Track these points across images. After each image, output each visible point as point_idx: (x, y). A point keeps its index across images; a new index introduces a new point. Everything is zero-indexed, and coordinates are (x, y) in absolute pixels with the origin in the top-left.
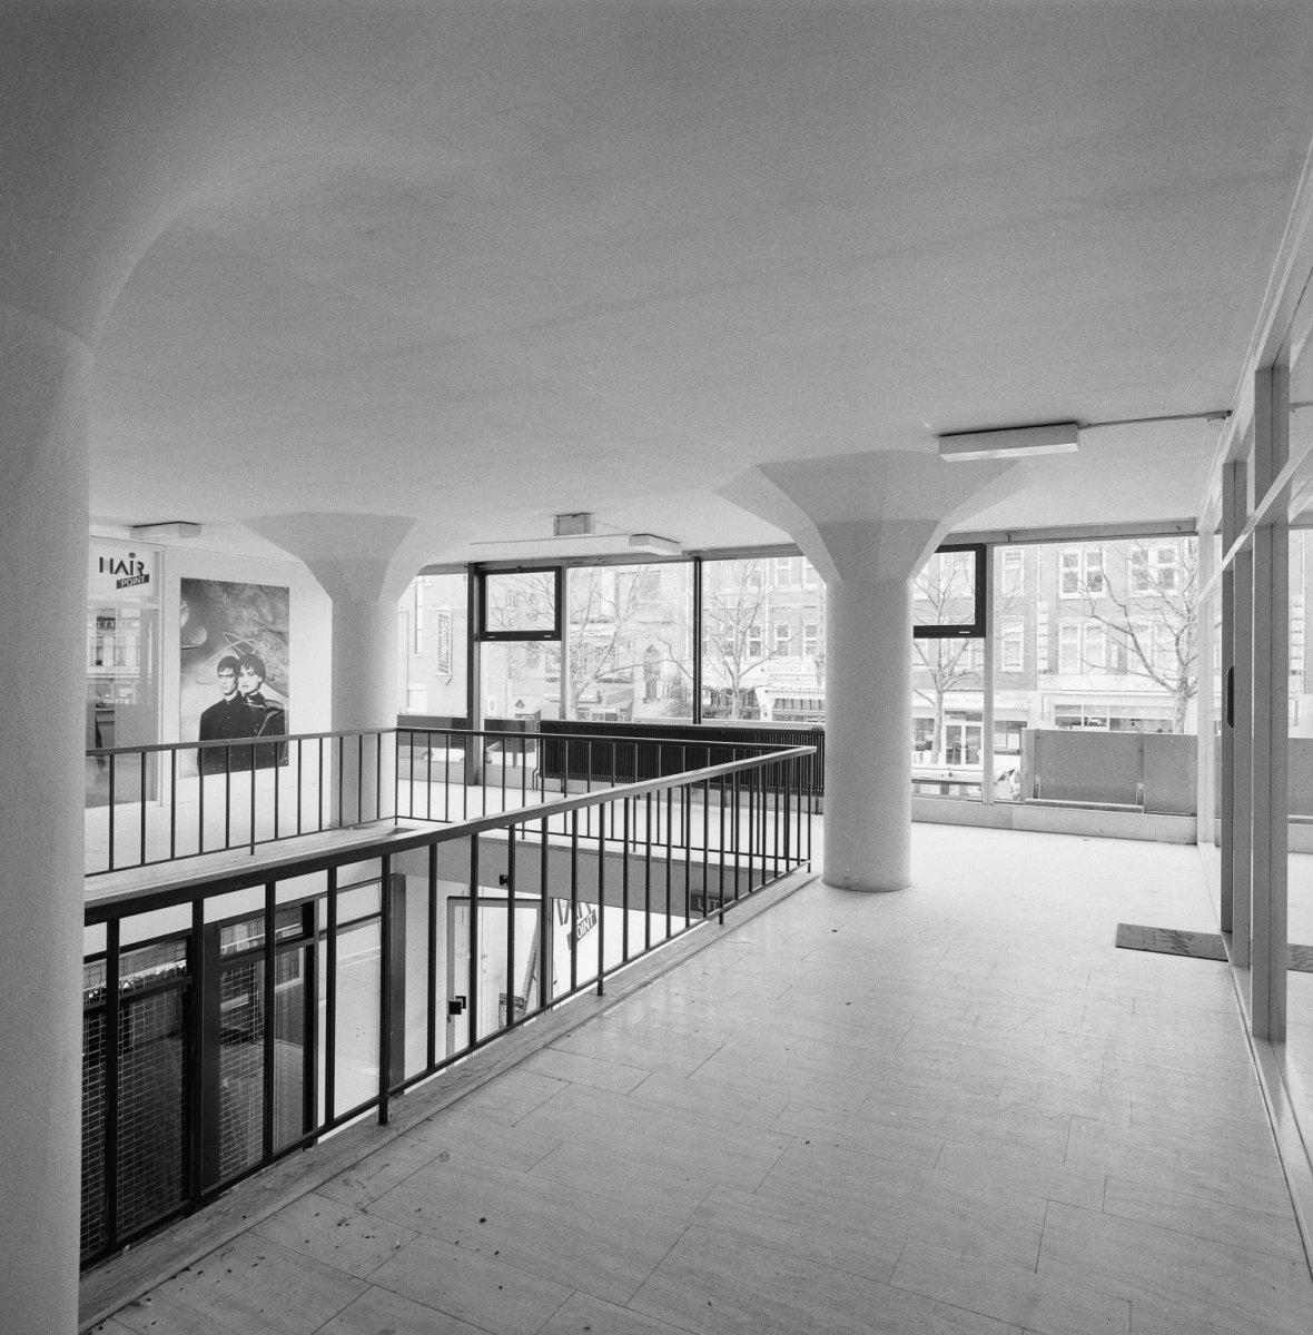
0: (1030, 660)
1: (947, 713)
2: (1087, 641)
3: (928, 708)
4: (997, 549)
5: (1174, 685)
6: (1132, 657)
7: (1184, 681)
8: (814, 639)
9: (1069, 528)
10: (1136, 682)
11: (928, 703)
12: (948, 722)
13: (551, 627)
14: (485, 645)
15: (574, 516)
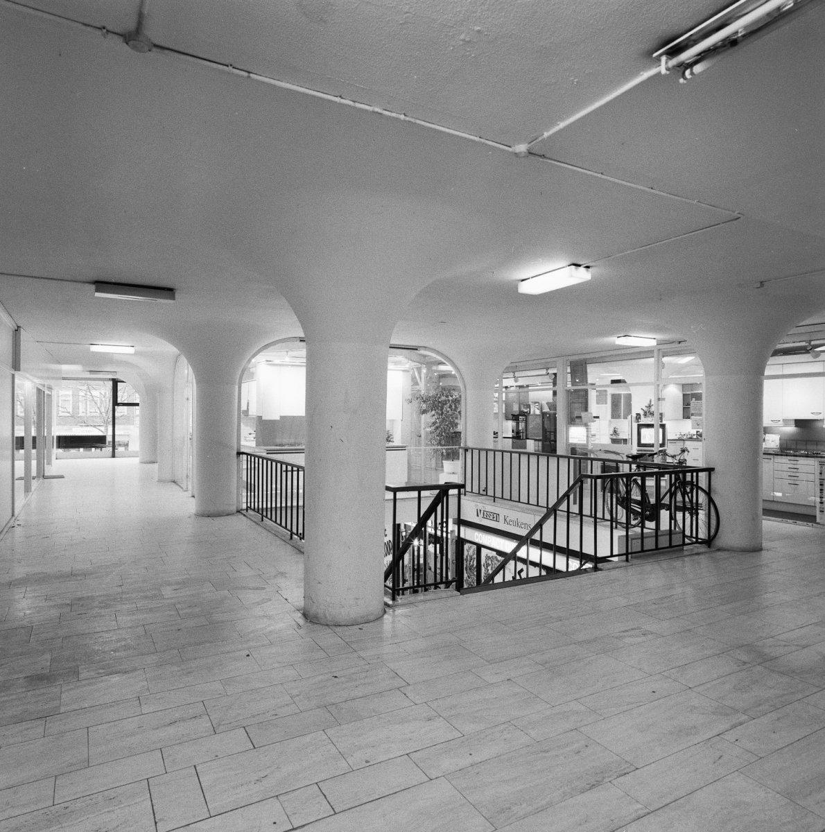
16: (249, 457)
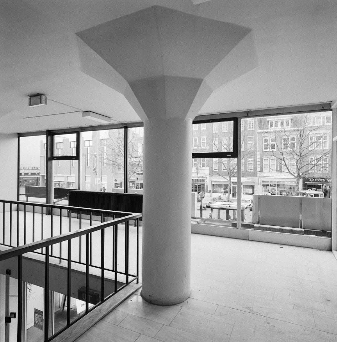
0: (255, 168)
1: (233, 183)
2: (271, 163)
3: (226, 181)
4: (243, 120)
5: (296, 175)
6: (284, 167)
7: (298, 174)
8: (196, 162)
10: (285, 175)
11: (227, 180)
12: (232, 186)
13: (75, 154)
14: (54, 162)
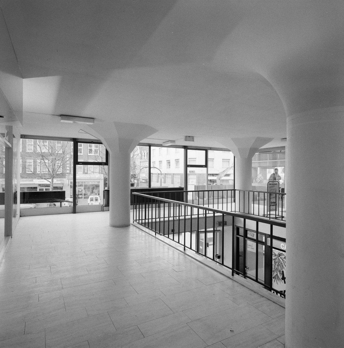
9: (221, 148)
15: (189, 137)
16: (204, 210)
